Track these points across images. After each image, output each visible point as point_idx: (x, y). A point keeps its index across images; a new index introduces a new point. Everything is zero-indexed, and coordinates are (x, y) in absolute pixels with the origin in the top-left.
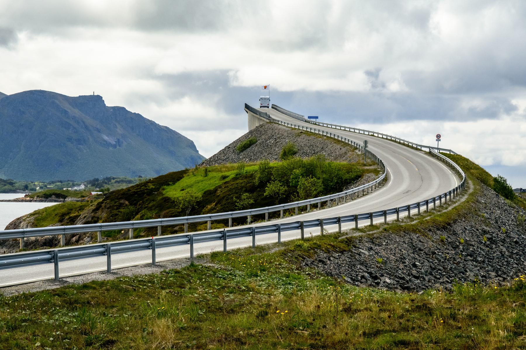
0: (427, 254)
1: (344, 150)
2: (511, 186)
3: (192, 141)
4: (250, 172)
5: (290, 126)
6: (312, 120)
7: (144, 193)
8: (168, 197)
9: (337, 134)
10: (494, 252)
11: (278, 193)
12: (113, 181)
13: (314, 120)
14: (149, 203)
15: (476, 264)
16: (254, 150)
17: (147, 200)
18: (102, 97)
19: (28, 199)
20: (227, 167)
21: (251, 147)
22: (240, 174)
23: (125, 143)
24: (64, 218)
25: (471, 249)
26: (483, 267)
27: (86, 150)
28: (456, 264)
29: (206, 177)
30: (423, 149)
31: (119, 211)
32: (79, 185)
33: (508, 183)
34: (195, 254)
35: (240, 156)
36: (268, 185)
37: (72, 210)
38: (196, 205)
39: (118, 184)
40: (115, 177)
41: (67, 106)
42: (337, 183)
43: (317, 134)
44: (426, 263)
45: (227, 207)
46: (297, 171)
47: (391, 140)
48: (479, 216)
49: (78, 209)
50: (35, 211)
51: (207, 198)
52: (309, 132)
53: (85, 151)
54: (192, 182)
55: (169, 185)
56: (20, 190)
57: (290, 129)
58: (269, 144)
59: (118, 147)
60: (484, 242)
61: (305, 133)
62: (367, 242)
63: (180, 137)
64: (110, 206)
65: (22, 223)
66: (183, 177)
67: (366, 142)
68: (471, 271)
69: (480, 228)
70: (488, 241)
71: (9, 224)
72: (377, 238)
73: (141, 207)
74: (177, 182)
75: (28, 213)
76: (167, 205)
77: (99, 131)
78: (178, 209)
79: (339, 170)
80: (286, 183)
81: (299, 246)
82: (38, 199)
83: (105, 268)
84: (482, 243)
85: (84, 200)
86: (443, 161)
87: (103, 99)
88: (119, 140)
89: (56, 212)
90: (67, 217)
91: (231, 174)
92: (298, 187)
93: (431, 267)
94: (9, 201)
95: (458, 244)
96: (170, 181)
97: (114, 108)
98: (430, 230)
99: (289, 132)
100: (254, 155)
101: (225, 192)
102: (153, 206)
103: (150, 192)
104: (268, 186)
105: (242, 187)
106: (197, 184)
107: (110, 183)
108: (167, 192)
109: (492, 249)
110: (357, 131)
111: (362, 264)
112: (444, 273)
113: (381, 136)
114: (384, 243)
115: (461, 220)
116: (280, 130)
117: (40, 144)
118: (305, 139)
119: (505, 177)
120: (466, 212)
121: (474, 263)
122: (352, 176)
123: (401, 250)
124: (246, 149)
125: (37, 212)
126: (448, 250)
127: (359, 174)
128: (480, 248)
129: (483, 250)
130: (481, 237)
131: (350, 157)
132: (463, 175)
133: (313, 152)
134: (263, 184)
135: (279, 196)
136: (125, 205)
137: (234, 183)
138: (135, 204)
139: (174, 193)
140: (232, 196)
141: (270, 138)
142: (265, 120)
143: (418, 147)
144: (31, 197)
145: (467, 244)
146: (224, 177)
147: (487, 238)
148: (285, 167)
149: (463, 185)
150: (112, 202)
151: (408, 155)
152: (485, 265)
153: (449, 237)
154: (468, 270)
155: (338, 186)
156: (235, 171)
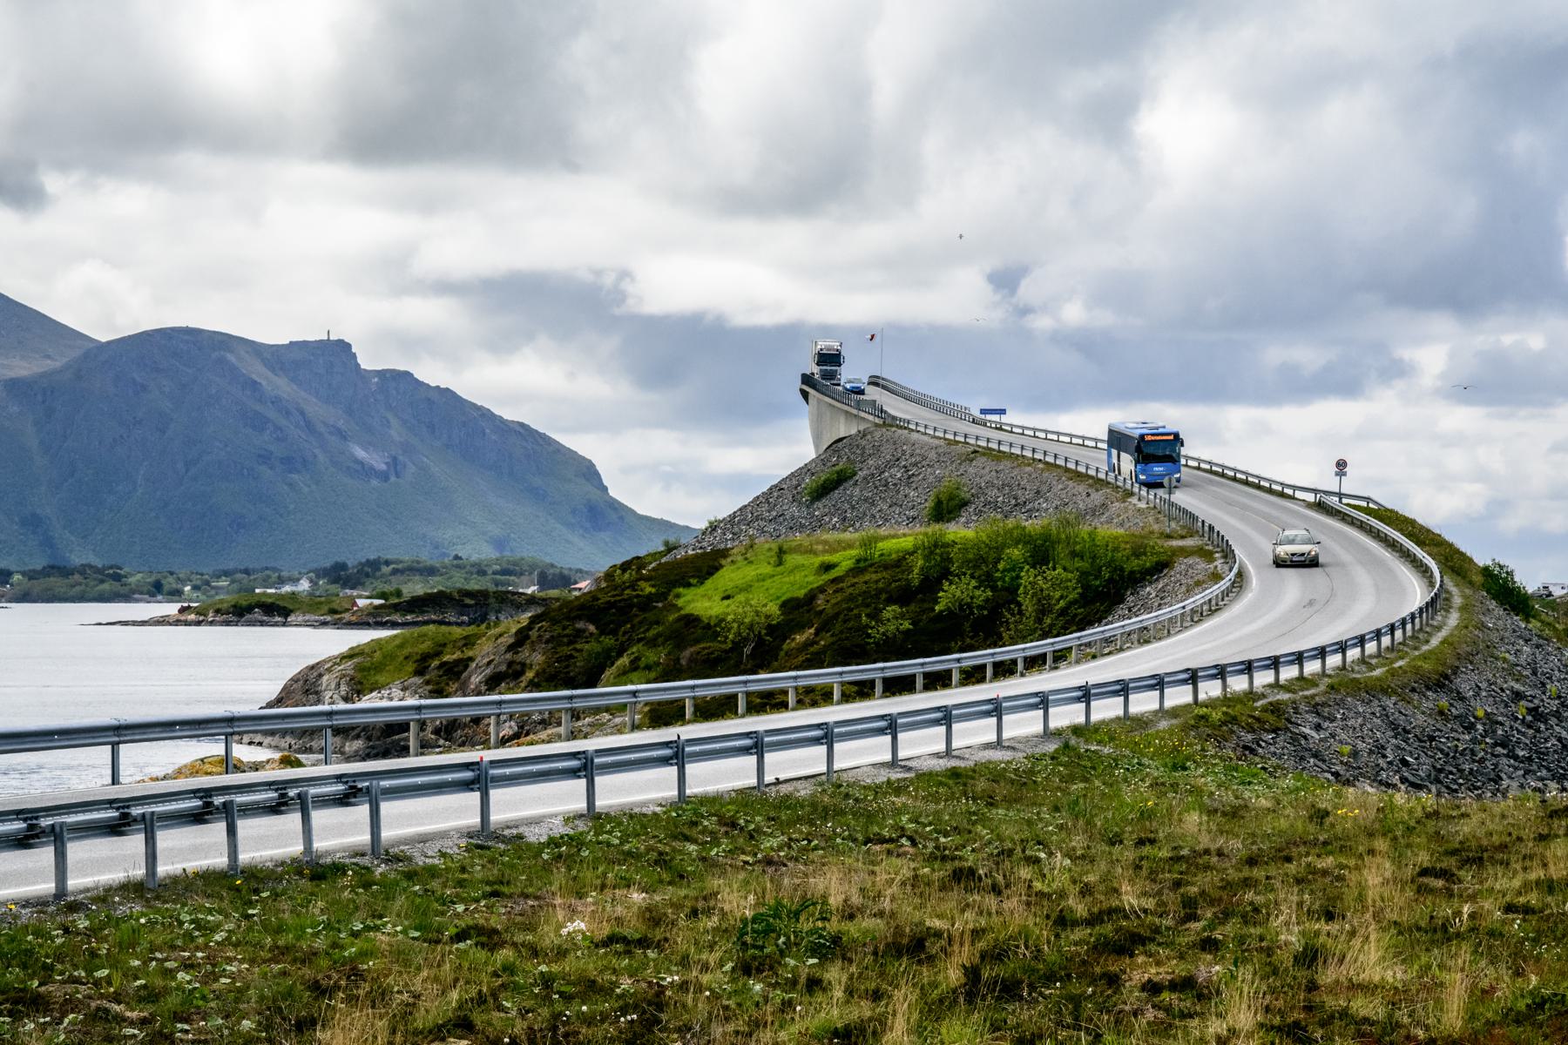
0: (1420, 741)
1: (1097, 497)
2: (1524, 588)
3: (590, 461)
4: (890, 555)
5: (941, 435)
6: (989, 417)
7: (631, 606)
8: (692, 615)
9: (1083, 460)
10: (1545, 739)
11: (969, 606)
12: (386, 569)
13: (995, 418)
14: (648, 630)
15: (1517, 764)
16: (851, 496)
17: (641, 623)
18: (349, 346)
19: (192, 617)
20: (825, 542)
21: (842, 488)
22: (866, 560)
23: (412, 469)
24: (427, 664)
25: (1500, 732)
26: (1530, 771)
27: (309, 486)
28: (1477, 762)
29: (782, 567)
31: (575, 649)
32: (296, 581)
33: (1516, 579)
35: (815, 510)
36: (946, 585)
37: (444, 645)
38: (766, 635)
39: (401, 578)
40: (389, 557)
41: (257, 371)
42: (1111, 580)
43: (1018, 455)
44: (1423, 759)
45: (847, 639)
46: (1016, 553)
47: (1211, 472)
48: (1497, 659)
49: (461, 644)
50: (352, 649)
51: (791, 617)
52: (994, 450)
53: (306, 490)
54: (747, 579)
55: (689, 585)
56: (141, 593)
57: (942, 442)
58: (890, 480)
59: (393, 479)
60: (1521, 717)
61: (984, 454)
62: (1307, 712)
63: (559, 451)
64: (552, 637)
65: (325, 678)
66: (722, 566)
68: (1510, 778)
69: (1505, 686)
70: (1529, 714)
71: (292, 679)
72: (1324, 704)
73: (628, 640)
74: (707, 579)
75: (336, 653)
76: (693, 633)
77: (343, 436)
78: (725, 642)
79: (1116, 549)
80: (987, 580)
81: (1202, 717)
82: (217, 619)
83: (888, 757)
84: (1517, 718)
85: (340, 619)
86: (1362, 526)
87: (353, 350)
88: (395, 459)
89: (406, 652)
90: (436, 663)
91: (845, 560)
92: (1021, 590)
93: (1434, 767)
94: (143, 623)
95: (1473, 720)
96: (693, 577)
97: (381, 374)
98: (1413, 690)
99: (941, 450)
100: (853, 508)
101: (837, 604)
102: (659, 635)
103: (646, 603)
104: (945, 588)
105: (879, 592)
106: (761, 584)
107: (378, 574)
108: (689, 602)
109: (1538, 731)
110: (1042, 435)
112: (1461, 781)
114: (1339, 716)
115: (1466, 668)
116: (917, 446)
117: (187, 471)
118: (987, 470)
119: (1510, 562)
120: (1469, 649)
121: (1512, 761)
122: (1148, 564)
123: (1372, 731)
124: (827, 494)
125: (357, 651)
126: (1456, 731)
127: (1163, 558)
128: (1517, 729)
129: (1524, 734)
130: (1513, 705)
131: (1119, 516)
133: (1013, 502)
134: (931, 585)
135: (973, 614)
136: (587, 634)
137: (855, 580)
138: (614, 632)
139: (707, 604)
140: (855, 612)
141: (889, 465)
142: (871, 418)
143: (1286, 491)
144: (198, 613)
145: (1490, 719)
146: (827, 567)
147: (1527, 708)
148: (984, 543)
150: (555, 627)
151: (1274, 513)
152: (1535, 767)
153: (1451, 705)
154: (1504, 776)
155: (1114, 588)
156: (854, 552)
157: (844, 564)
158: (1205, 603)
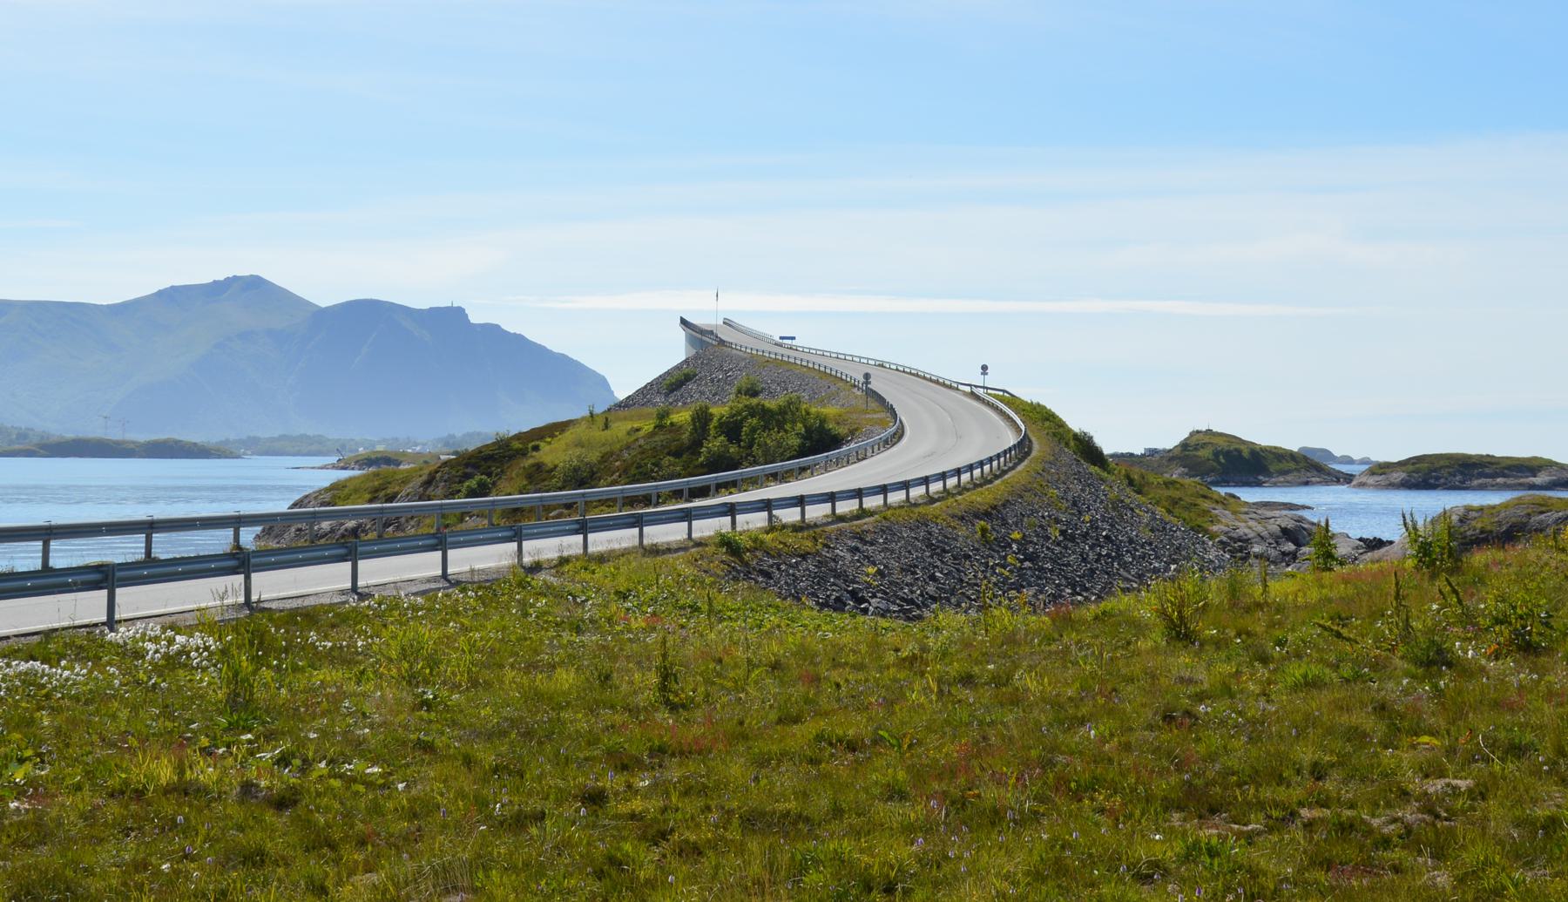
9: (835, 368)
13: (789, 342)
18: (464, 310)
25: (1031, 550)
30: (961, 387)
34: (527, 560)
47: (910, 373)
67: (867, 376)
86: (996, 409)
111: (837, 576)
113: (894, 367)
132: (1023, 428)
134: (696, 445)
149: (1020, 443)
157: (646, 427)
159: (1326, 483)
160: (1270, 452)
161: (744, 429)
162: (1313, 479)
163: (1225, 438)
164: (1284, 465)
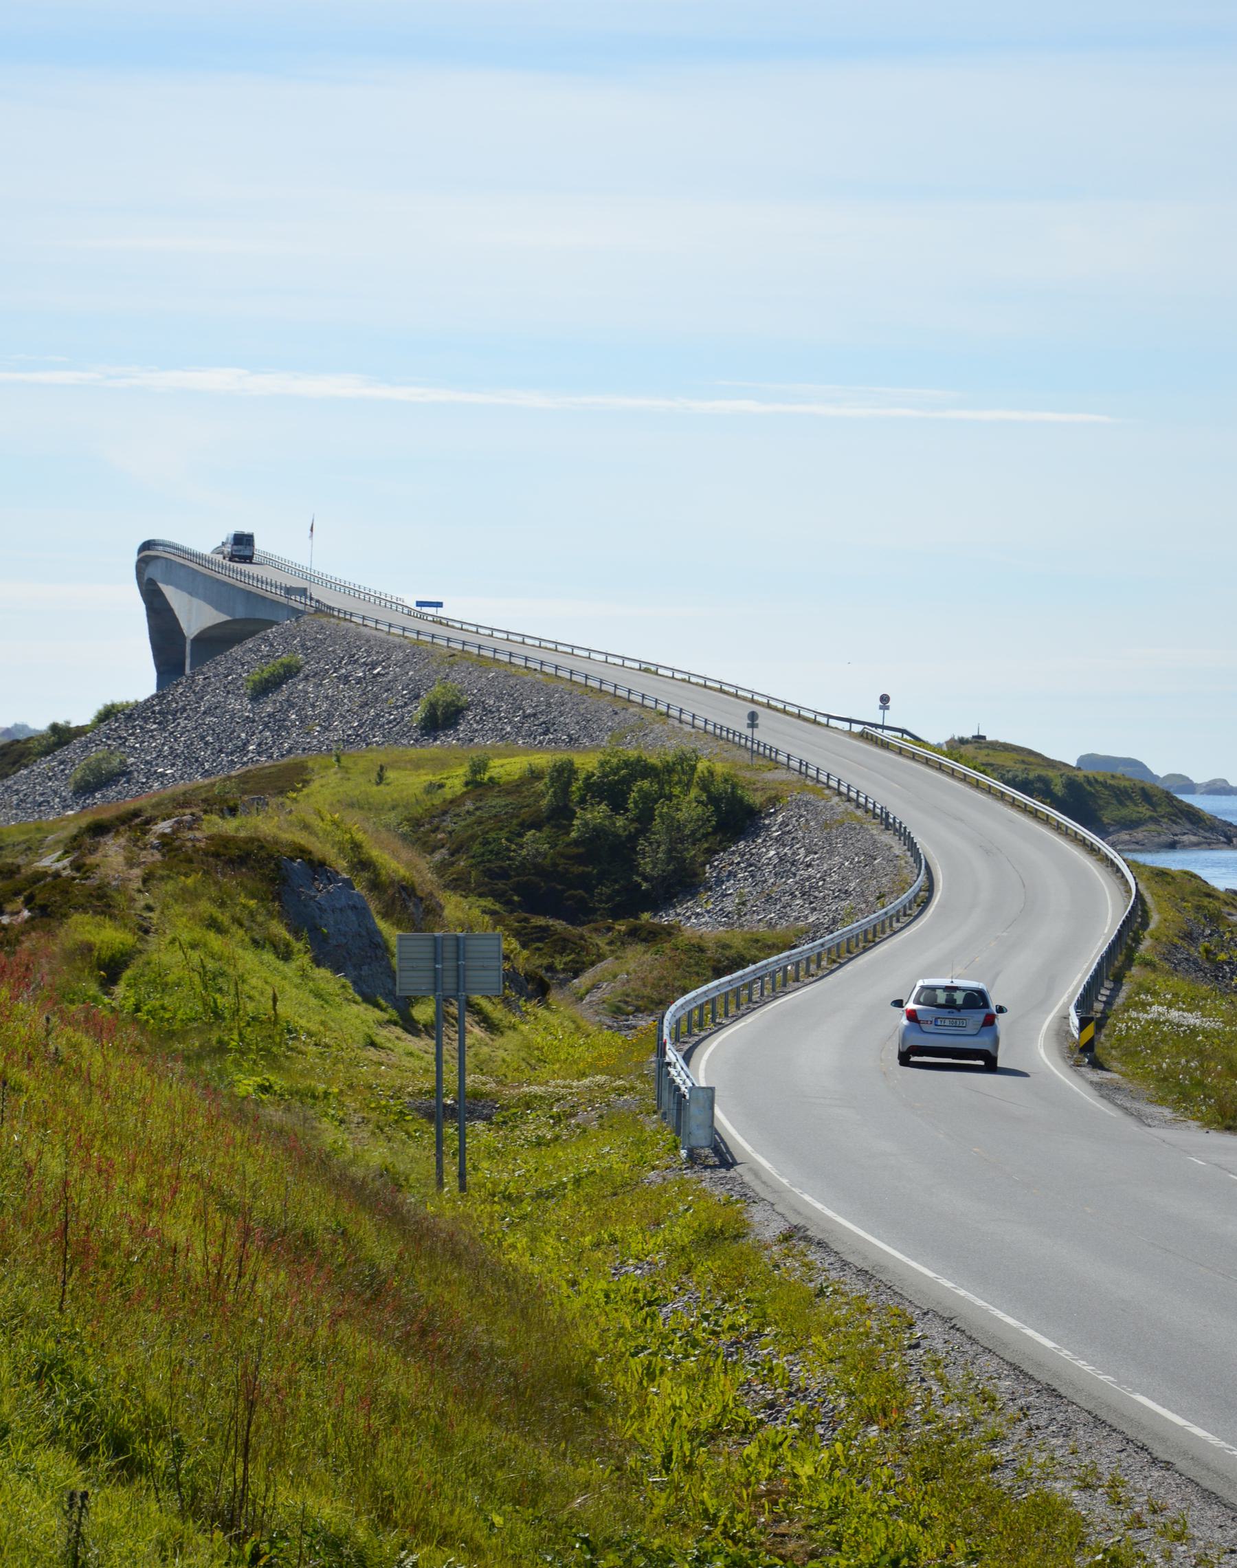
6: (425, 610)
86: (940, 768)
158: (707, 1002)
159: (1209, 845)
160: (1105, 785)
161: (633, 794)
162: (1185, 838)
163: (1014, 755)
164: (1131, 811)
